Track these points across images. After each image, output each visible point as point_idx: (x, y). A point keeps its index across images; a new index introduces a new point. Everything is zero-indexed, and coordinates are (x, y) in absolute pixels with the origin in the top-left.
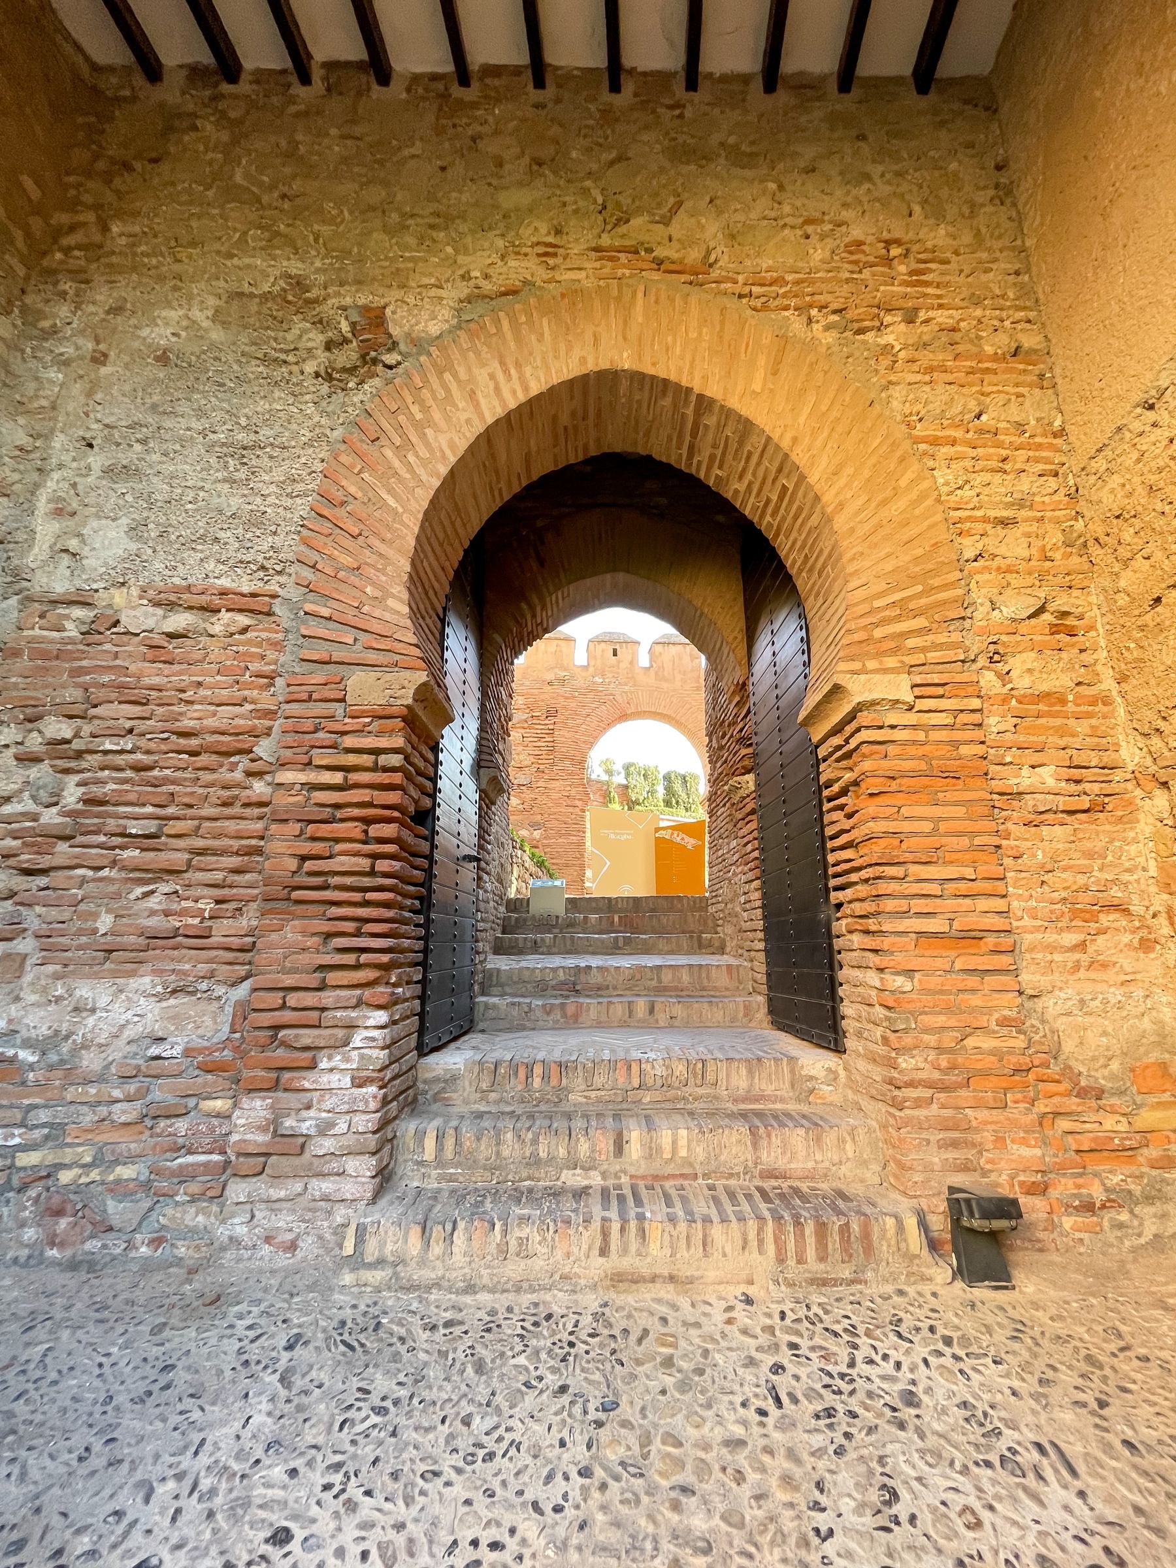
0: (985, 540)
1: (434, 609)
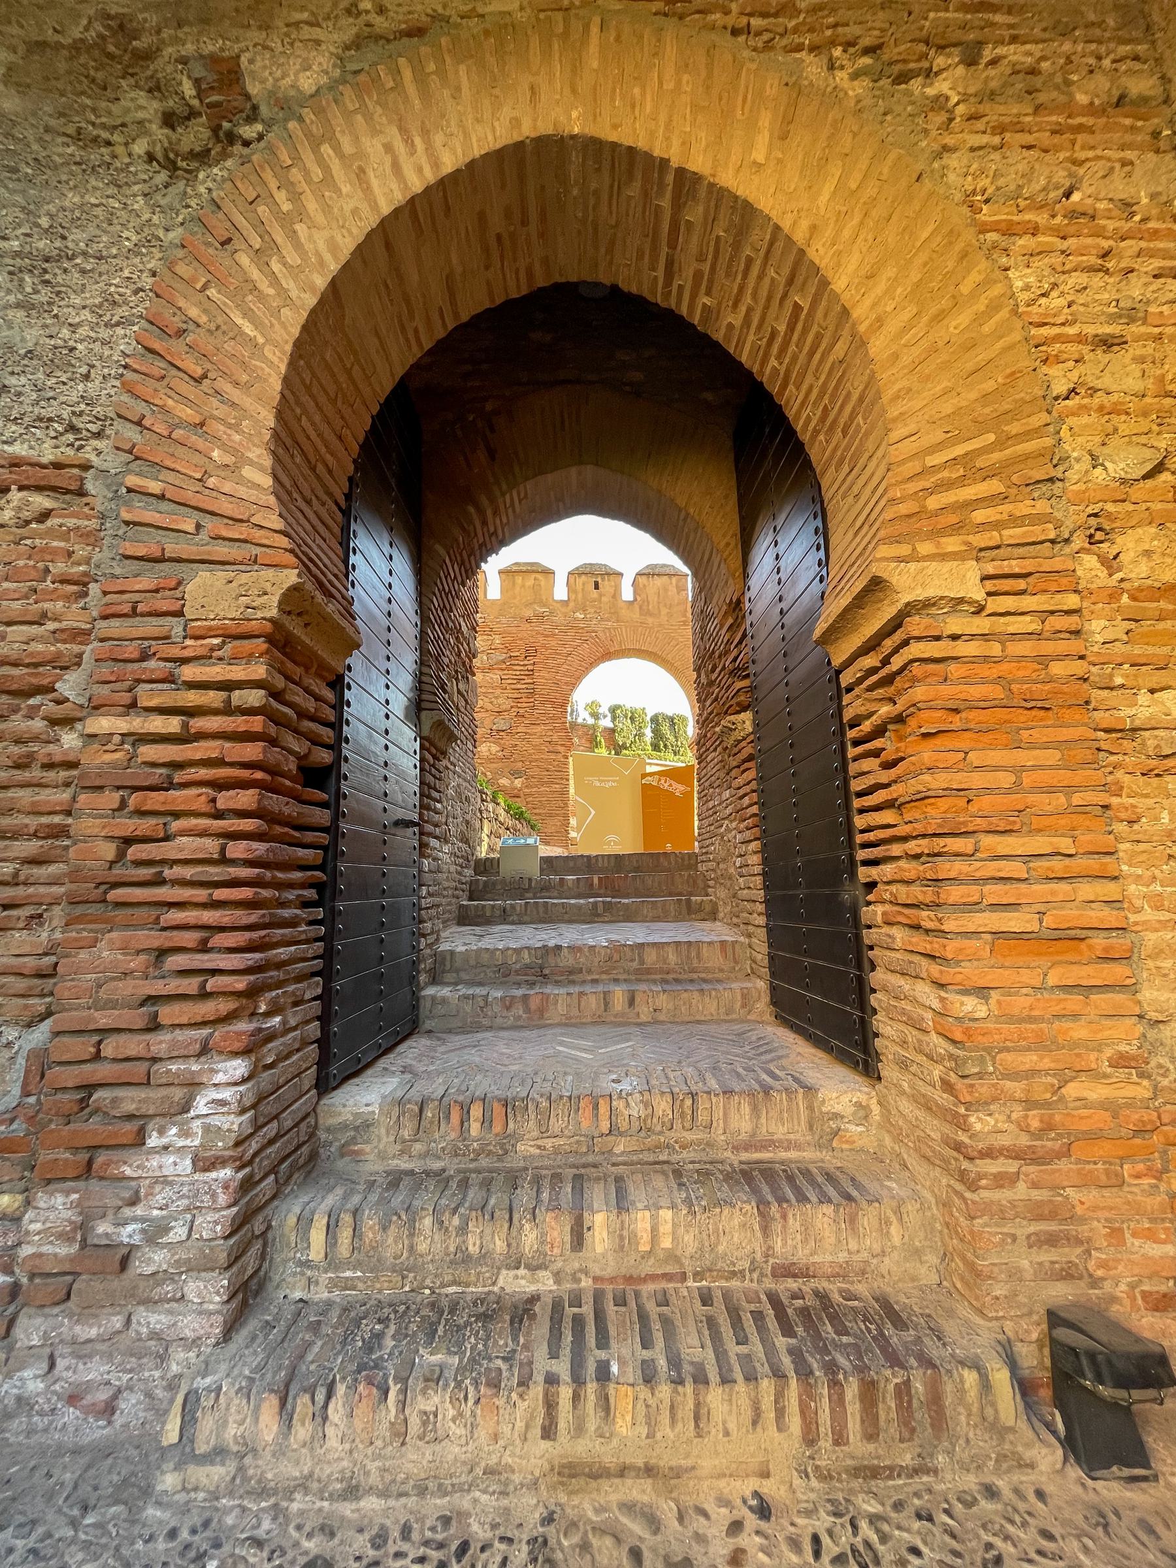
0: (1082, 368)
1: (330, 494)
